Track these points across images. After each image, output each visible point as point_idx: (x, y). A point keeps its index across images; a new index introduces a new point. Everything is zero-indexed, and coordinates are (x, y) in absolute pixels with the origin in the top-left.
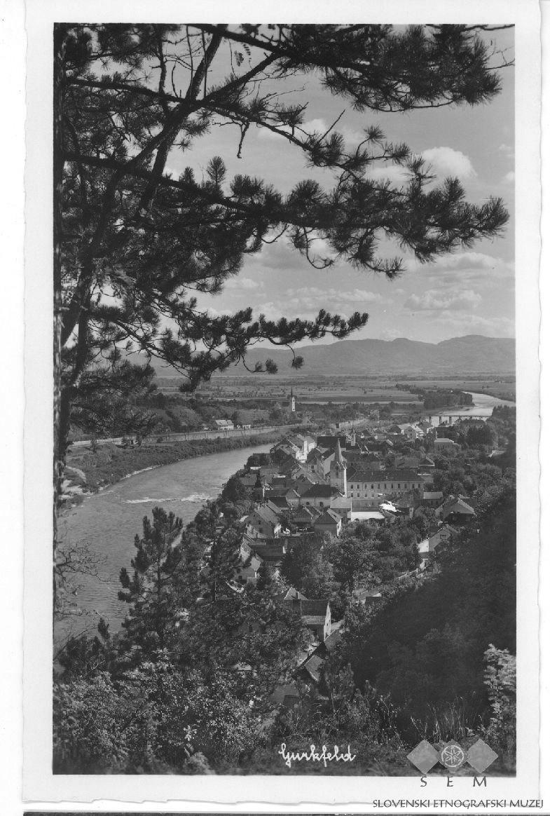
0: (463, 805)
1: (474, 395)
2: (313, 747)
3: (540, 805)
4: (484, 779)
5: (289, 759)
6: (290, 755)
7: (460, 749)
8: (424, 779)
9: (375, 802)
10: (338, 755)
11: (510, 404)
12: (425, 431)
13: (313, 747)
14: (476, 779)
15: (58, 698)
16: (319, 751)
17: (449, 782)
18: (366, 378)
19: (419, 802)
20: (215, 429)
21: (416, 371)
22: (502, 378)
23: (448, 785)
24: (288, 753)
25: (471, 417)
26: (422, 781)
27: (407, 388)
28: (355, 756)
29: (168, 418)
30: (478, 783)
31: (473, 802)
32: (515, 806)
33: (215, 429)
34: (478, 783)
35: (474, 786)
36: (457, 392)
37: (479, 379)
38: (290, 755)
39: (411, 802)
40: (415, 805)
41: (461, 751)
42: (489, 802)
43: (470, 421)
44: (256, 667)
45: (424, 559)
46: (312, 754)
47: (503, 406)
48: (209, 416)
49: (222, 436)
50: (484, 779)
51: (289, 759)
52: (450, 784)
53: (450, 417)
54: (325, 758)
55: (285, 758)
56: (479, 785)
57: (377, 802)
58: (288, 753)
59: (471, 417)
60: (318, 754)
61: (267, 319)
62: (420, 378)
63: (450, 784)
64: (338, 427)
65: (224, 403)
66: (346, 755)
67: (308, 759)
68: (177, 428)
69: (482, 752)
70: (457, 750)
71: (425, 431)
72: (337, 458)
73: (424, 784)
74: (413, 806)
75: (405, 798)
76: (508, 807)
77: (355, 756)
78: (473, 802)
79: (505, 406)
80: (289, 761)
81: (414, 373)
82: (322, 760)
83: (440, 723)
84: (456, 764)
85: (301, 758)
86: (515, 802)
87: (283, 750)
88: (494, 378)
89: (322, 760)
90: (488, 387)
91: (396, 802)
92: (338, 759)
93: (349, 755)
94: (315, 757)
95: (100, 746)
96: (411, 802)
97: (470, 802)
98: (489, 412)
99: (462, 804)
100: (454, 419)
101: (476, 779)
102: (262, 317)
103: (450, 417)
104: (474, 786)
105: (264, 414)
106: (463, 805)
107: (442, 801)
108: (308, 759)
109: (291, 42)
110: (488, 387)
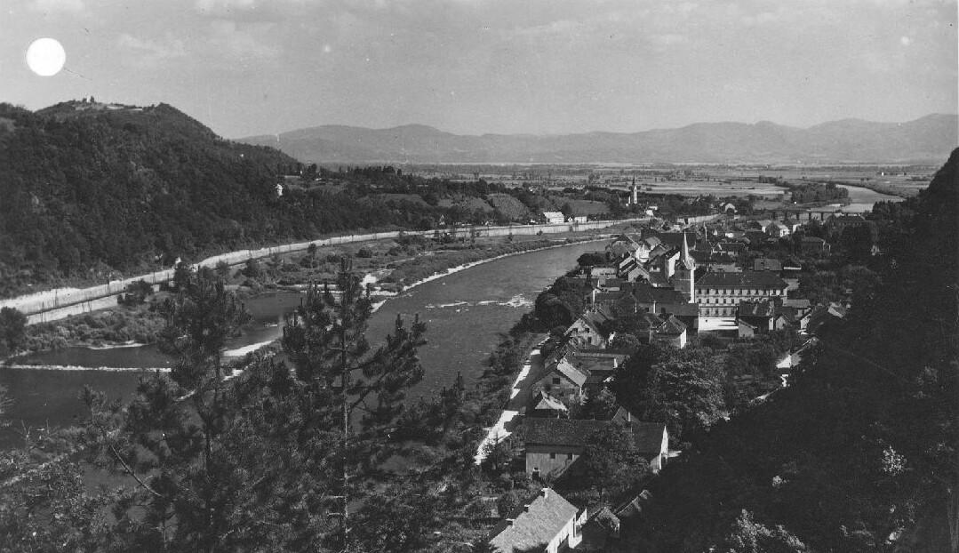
1: (850, 188)
12: (791, 229)
18: (724, 167)
20: (544, 221)
21: (781, 162)
22: (883, 169)
25: (847, 214)
27: (772, 181)
29: (488, 208)
33: (544, 221)
36: (831, 185)
37: (858, 169)
43: (847, 217)
44: (148, 205)
49: (545, 230)
53: (822, 213)
59: (847, 214)
65: (555, 193)
68: (501, 221)
71: (791, 229)
72: (682, 256)
81: (778, 163)
83: (299, 283)
90: (868, 179)
98: (113, 302)
100: (826, 216)
105: (599, 207)
109: (197, 535)
110: (868, 179)
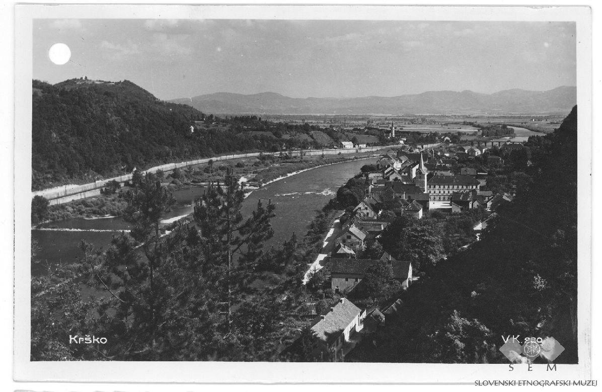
0: (540, 384)
1: (515, 128)
3: (595, 384)
4: (555, 366)
8: (511, 365)
9: (477, 382)
12: (482, 151)
14: (549, 366)
19: (508, 382)
20: (342, 146)
23: (529, 370)
26: (510, 367)
27: (471, 124)
29: (310, 140)
31: (547, 382)
32: (577, 385)
33: (342, 146)
35: (548, 370)
36: (504, 126)
39: (502, 382)
40: (505, 384)
47: (536, 136)
48: (338, 139)
50: (555, 366)
52: (530, 369)
53: (499, 142)
56: (551, 370)
57: (478, 382)
61: (330, 314)
62: (538, 7)
63: (530, 369)
64: (423, 148)
65: (348, 131)
68: (318, 147)
69: (549, 346)
71: (482, 151)
72: (420, 167)
73: (511, 369)
74: (503, 385)
75: (497, 379)
76: (572, 385)
78: (547, 382)
79: (537, 136)
84: (534, 354)
86: (577, 382)
88: (529, 117)
90: (525, 123)
91: (491, 382)
95: (88, 80)
96: (502, 382)
97: (545, 382)
99: (539, 383)
100: (502, 144)
101: (549, 366)
102: (326, 334)
103: (499, 142)
104: (548, 370)
106: (540, 384)
110: (525, 123)
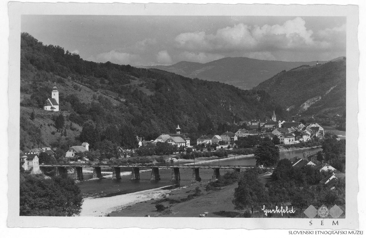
2: (277, 207)
5: (266, 212)
6: (267, 211)
7: (327, 209)
10: (288, 211)
11: (43, 165)
13: (277, 207)
15: (21, 203)
16: (279, 208)
17: (322, 223)
23: (322, 225)
24: (266, 210)
28: (295, 211)
30: (335, 224)
31: (333, 232)
34: (335, 224)
35: (333, 225)
38: (267, 211)
40: (307, 233)
41: (327, 210)
42: (339, 232)
45: (234, 124)
46: (276, 210)
51: (266, 212)
52: (322, 224)
54: (282, 212)
55: (265, 212)
56: (335, 224)
57: (290, 232)
58: (266, 210)
60: (279, 210)
63: (322, 224)
66: (291, 210)
67: (275, 212)
70: (325, 209)
73: (311, 224)
74: (306, 234)
77: (295, 211)
78: (333, 232)
80: (266, 213)
82: (281, 212)
85: (272, 212)
86: (351, 232)
87: (264, 208)
89: (281, 212)
92: (288, 212)
93: (292, 211)
94: (278, 211)
97: (331, 232)
104: (333, 225)
107: (319, 231)
108: (275, 212)
